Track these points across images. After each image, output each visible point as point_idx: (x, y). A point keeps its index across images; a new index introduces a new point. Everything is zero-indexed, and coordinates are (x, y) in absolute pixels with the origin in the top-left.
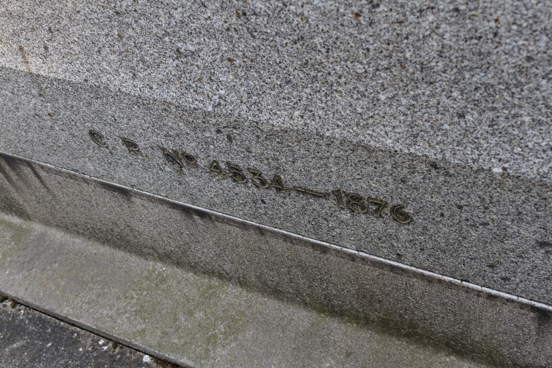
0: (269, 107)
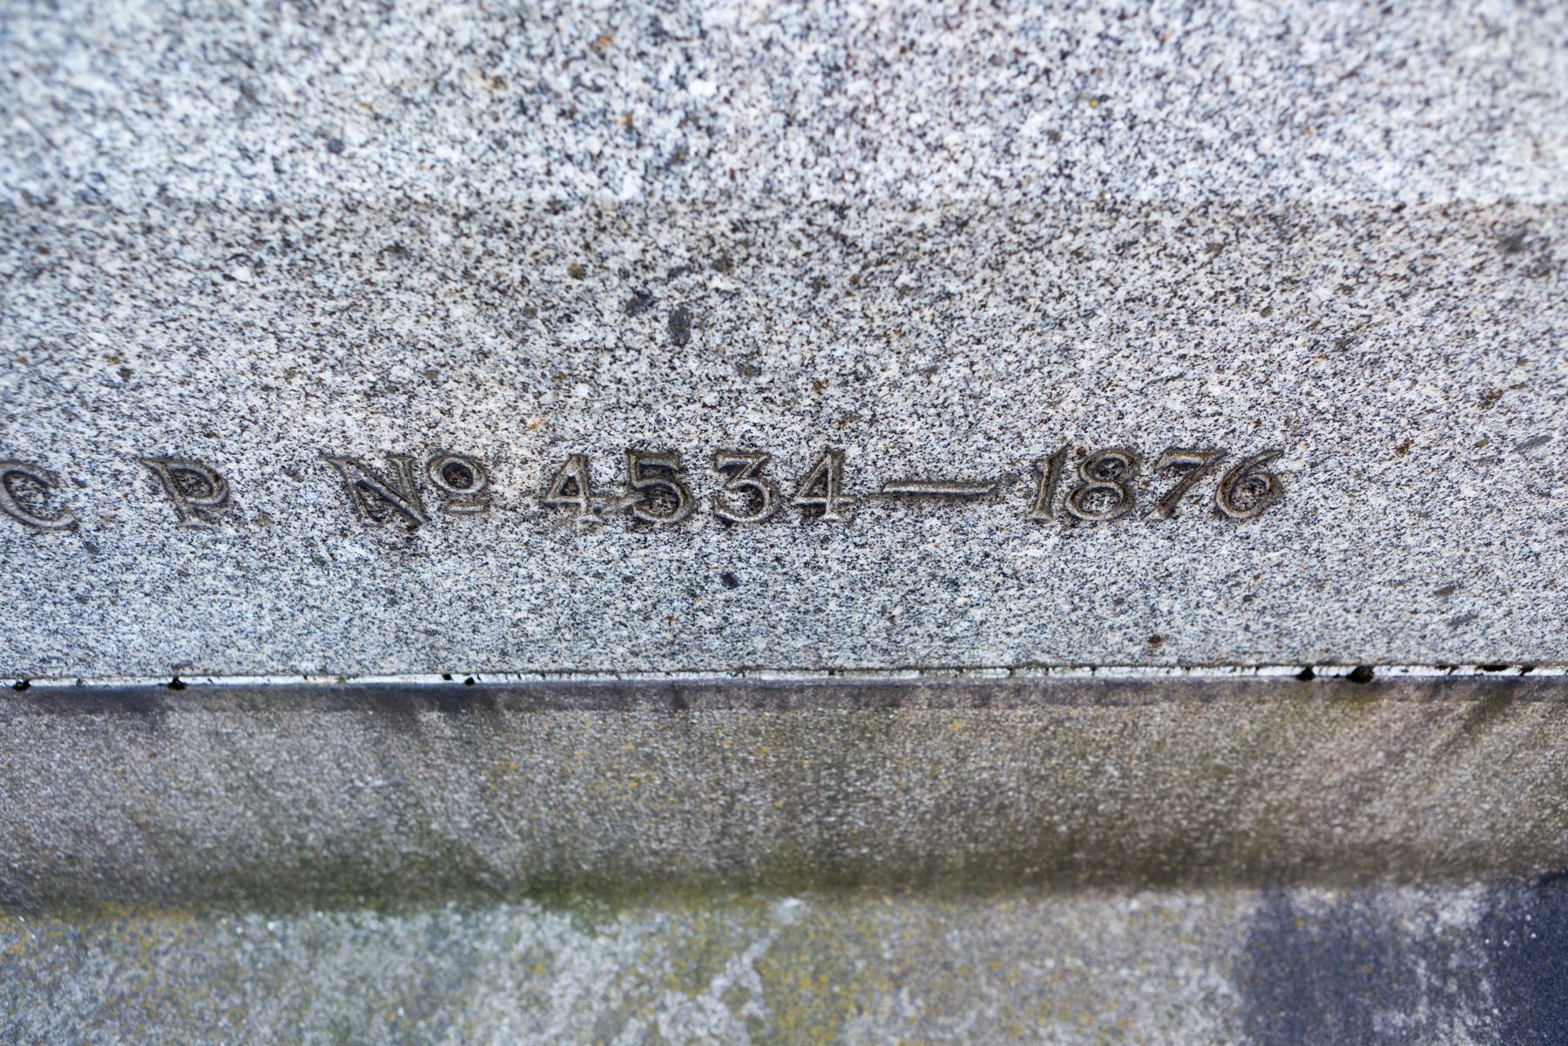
0: (917, 119)
